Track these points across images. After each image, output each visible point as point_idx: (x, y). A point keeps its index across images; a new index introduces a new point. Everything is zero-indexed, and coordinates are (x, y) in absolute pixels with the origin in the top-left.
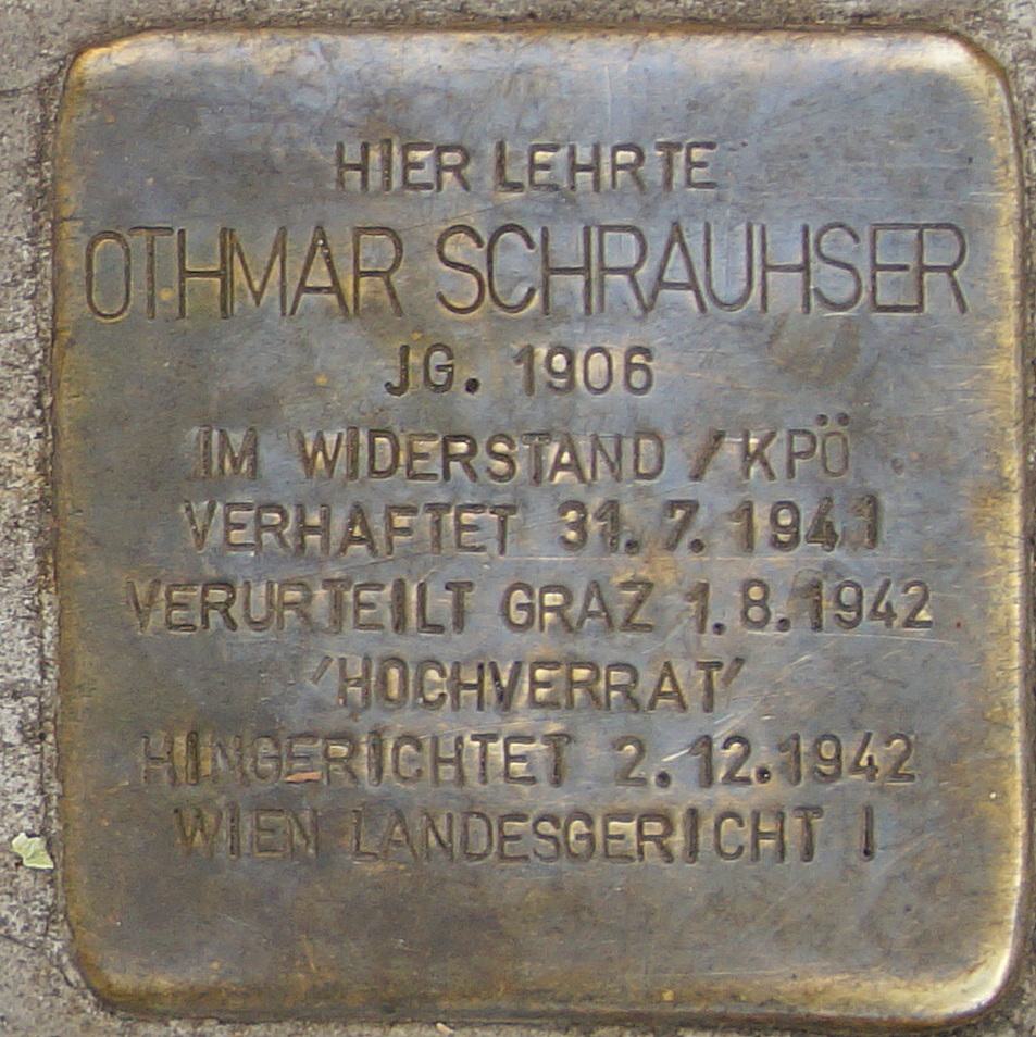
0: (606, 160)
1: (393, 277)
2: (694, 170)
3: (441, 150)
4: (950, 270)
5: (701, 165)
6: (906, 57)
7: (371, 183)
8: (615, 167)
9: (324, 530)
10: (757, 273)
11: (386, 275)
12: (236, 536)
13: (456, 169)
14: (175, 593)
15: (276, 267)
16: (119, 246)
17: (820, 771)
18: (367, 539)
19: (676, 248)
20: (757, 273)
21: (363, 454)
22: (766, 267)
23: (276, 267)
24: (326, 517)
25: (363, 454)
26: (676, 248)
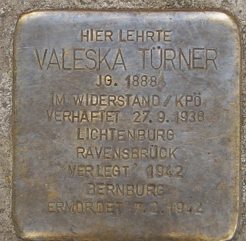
0: (145, 35)
1: (173, 60)
2: (98, 37)
3: (106, 31)
4: (213, 60)
5: (100, 36)
6: (46, 15)
7: (144, 40)
8: (147, 36)
9: (78, 117)
10: (163, 60)
11: (172, 60)
12: (58, 118)
13: (151, 37)
14: (120, 133)
15: (182, 58)
16: (173, 53)
17: (158, 174)
18: (87, 118)
19: (54, 55)
20: (163, 60)
21: (89, 100)
22: (165, 59)
23: (182, 58)
24: (79, 114)
25: (89, 100)
26: (54, 55)
